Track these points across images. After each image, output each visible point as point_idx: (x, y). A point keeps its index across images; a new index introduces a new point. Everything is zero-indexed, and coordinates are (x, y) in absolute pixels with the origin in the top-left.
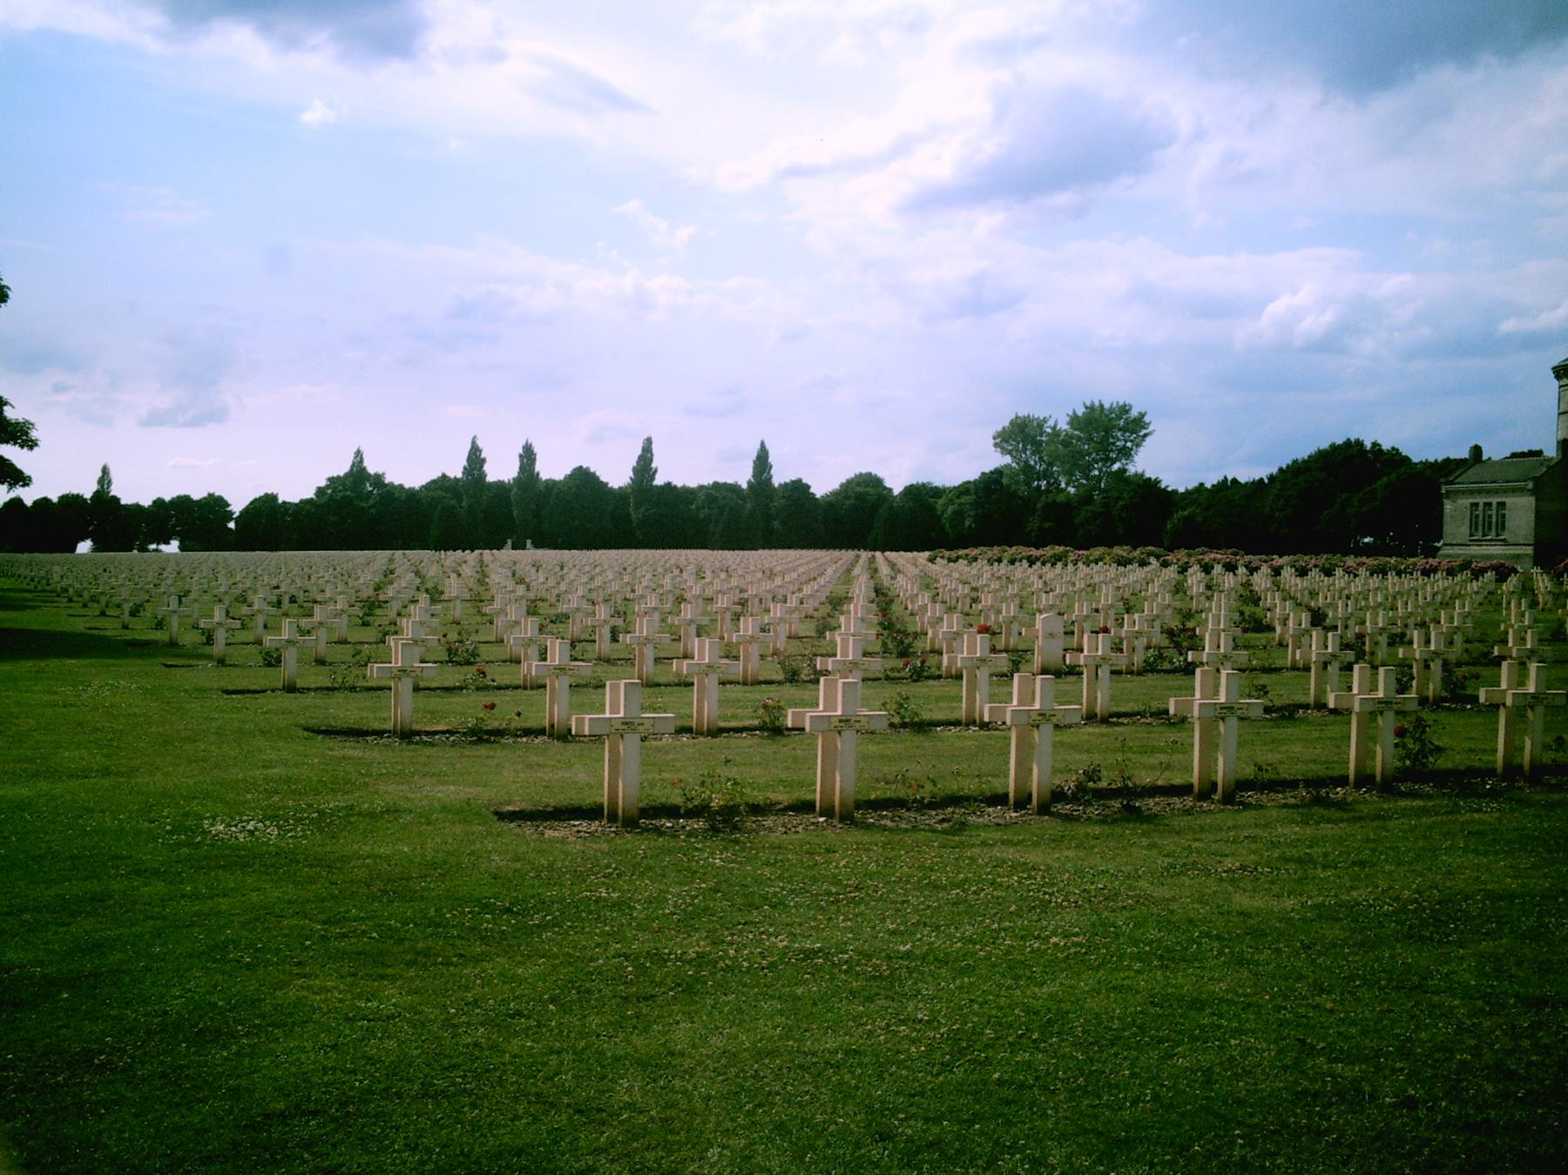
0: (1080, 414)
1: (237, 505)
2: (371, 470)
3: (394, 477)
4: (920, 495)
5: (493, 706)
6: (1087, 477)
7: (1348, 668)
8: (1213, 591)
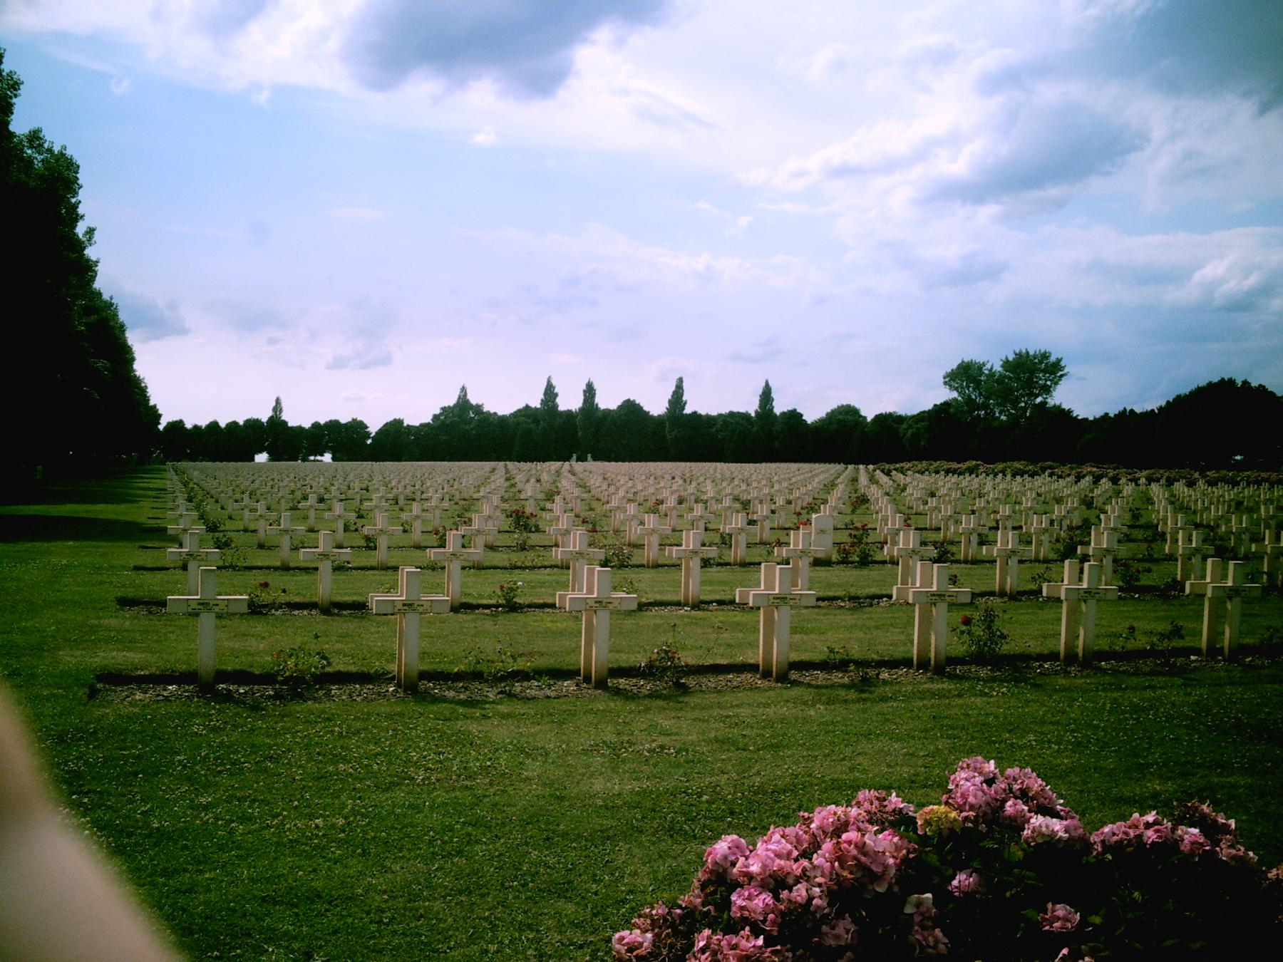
0: (1011, 359)
1: (374, 427)
2: (474, 402)
3: (489, 407)
4: (887, 422)
5: (266, 585)
6: (1015, 408)
7: (1204, 559)
8: (1116, 499)
